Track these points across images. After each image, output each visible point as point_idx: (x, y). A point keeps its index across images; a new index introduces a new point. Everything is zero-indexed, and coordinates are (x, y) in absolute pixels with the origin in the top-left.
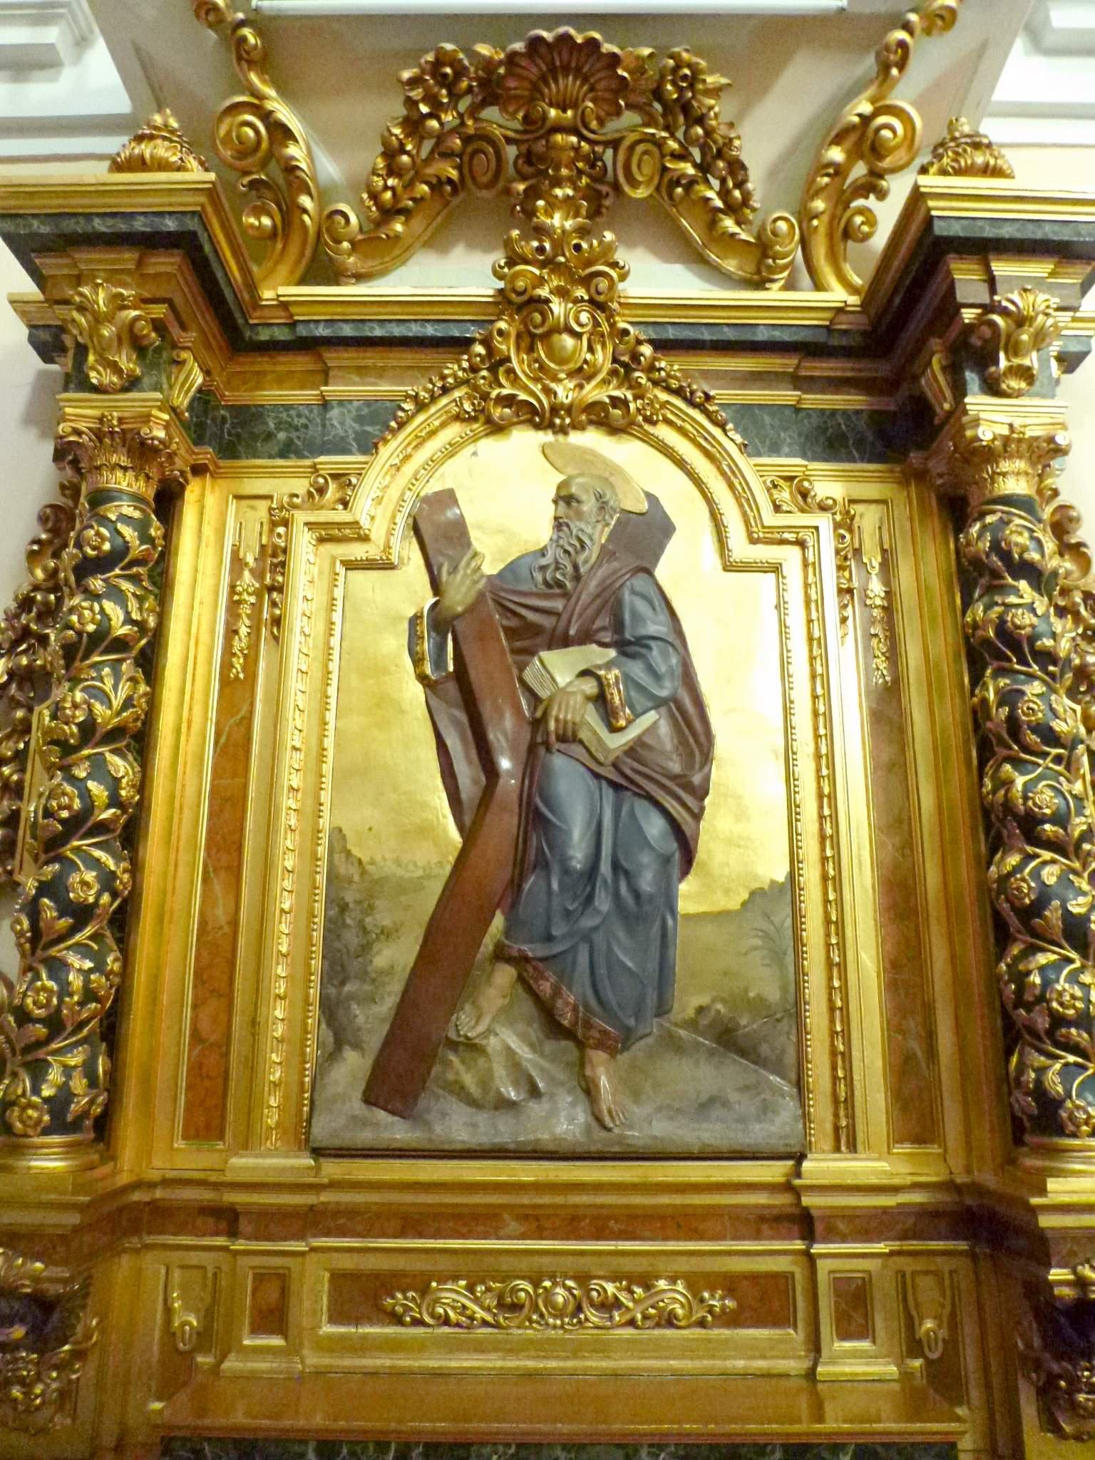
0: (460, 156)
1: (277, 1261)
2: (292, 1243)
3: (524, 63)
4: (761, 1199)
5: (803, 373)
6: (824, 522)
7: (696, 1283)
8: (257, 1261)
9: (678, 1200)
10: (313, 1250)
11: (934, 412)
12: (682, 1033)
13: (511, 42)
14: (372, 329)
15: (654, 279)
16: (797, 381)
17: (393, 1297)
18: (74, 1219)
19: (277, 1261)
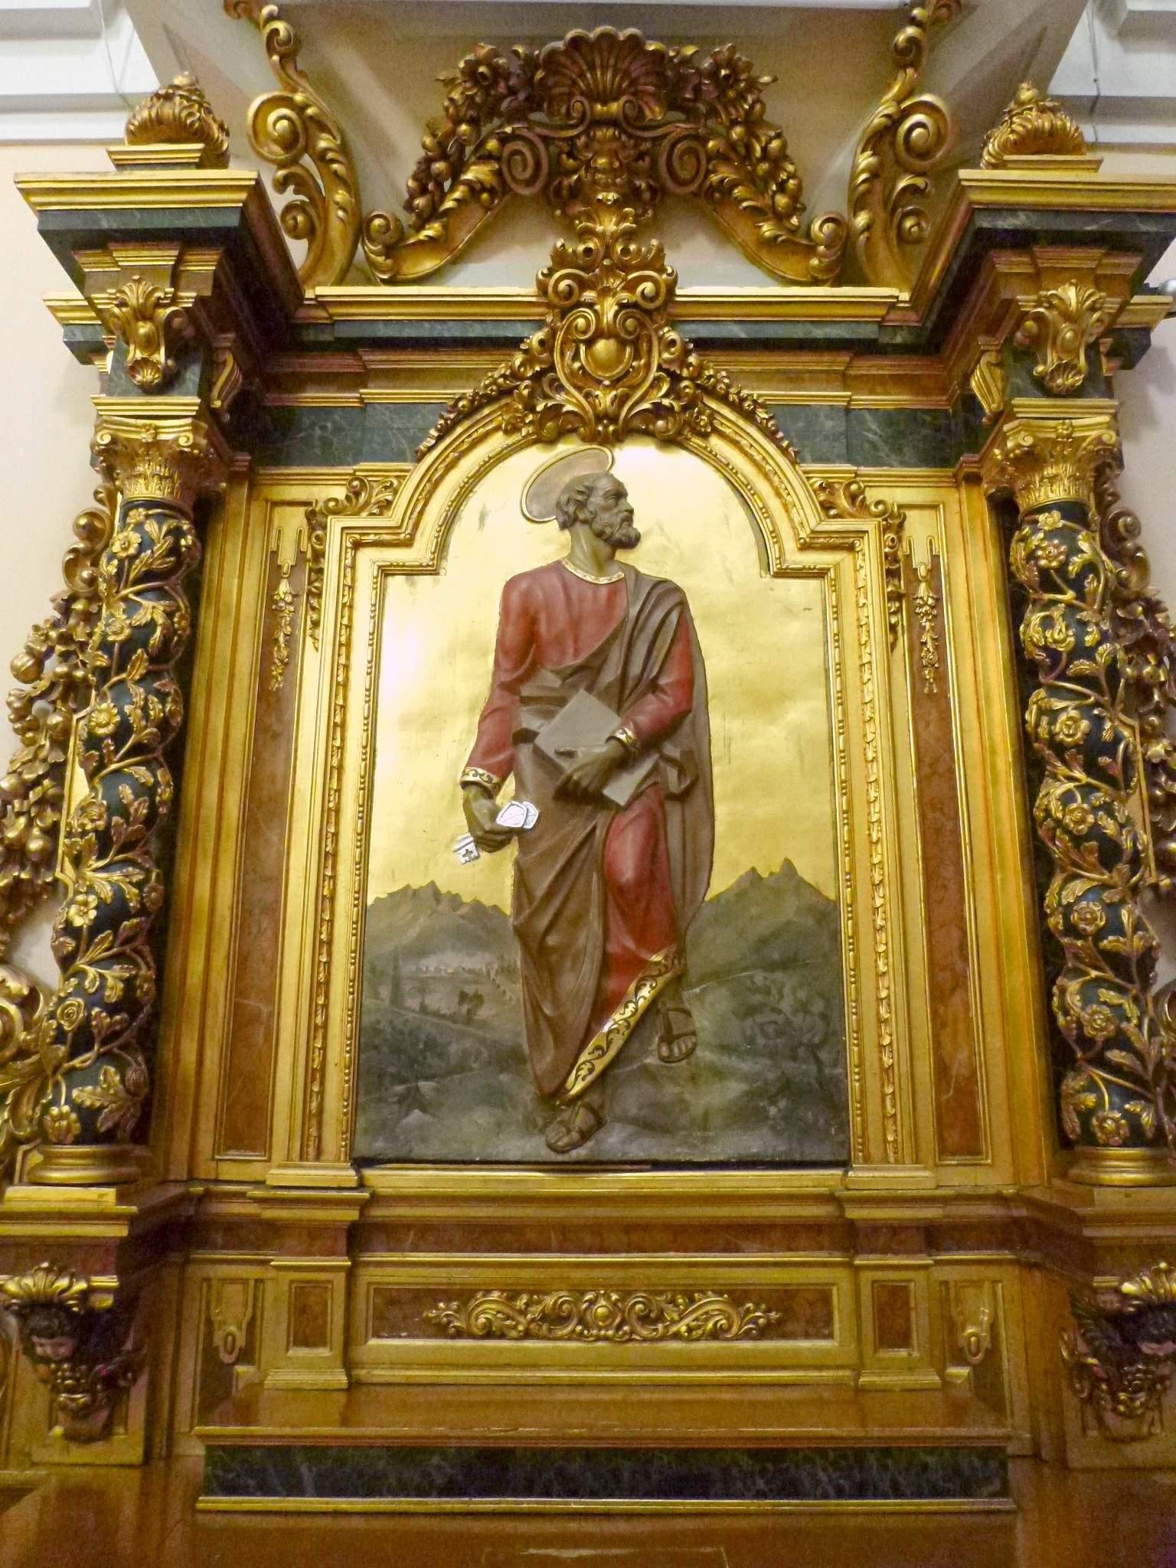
0: (498, 159)
1: (892, 1275)
2: (672, 1254)
3: (563, 59)
4: (986, 1210)
5: (853, 372)
6: (870, 525)
7: (737, 1296)
8: (879, 1275)
9: (591, 1212)
10: (937, 1263)
11: (981, 408)
12: (76, 1062)
13: (566, 32)
14: (449, 329)
15: (712, 274)
16: (845, 380)
17: (437, 1308)
18: (122, 1231)
19: (892, 1275)
